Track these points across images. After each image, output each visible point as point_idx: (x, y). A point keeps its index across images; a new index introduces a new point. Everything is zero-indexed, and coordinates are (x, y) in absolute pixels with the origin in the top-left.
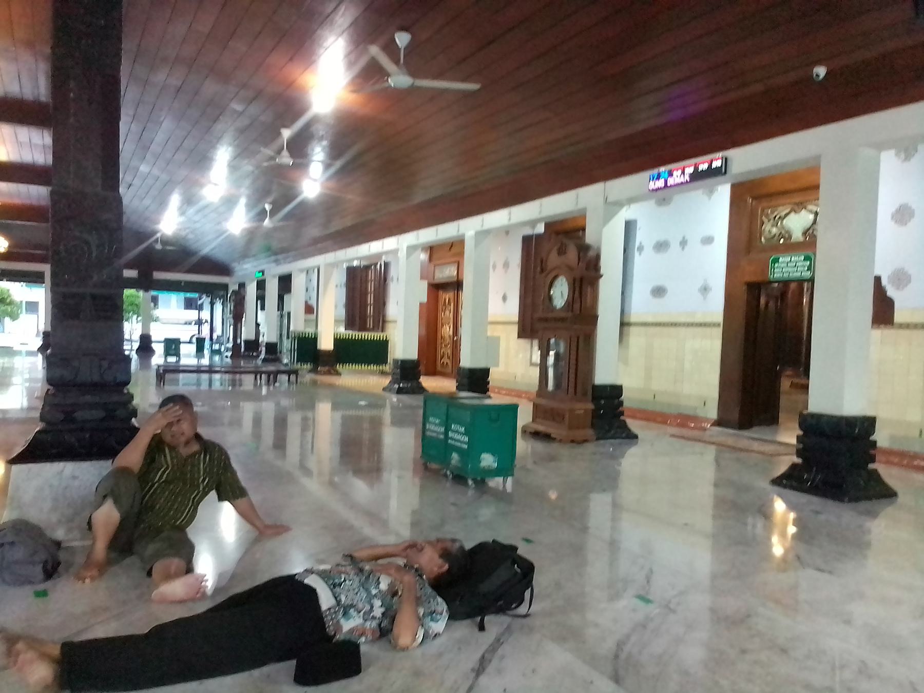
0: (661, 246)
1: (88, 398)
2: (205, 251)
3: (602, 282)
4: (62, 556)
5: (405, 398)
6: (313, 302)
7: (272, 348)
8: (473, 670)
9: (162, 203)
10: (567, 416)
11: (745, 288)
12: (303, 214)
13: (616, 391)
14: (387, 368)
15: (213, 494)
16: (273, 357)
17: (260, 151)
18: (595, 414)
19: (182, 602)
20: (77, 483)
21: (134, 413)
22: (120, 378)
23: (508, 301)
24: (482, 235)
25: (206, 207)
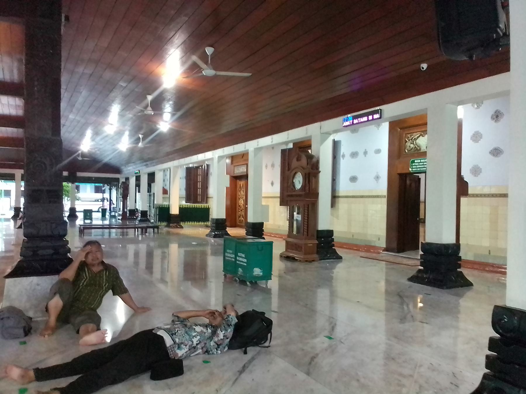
0: (354, 155)
1: (44, 244)
2: (106, 160)
3: (320, 174)
4: (33, 325)
5: (217, 240)
6: (167, 188)
7: (144, 214)
8: (238, 371)
9: (82, 135)
10: (303, 248)
11: (398, 176)
12: (160, 140)
13: (330, 233)
14: (209, 223)
15: (110, 292)
16: (145, 218)
17: (135, 107)
18: (318, 246)
19: (95, 345)
20: (39, 288)
21: (69, 251)
22: (62, 233)
23: (274, 185)
24: (258, 150)
25: (107, 136)
